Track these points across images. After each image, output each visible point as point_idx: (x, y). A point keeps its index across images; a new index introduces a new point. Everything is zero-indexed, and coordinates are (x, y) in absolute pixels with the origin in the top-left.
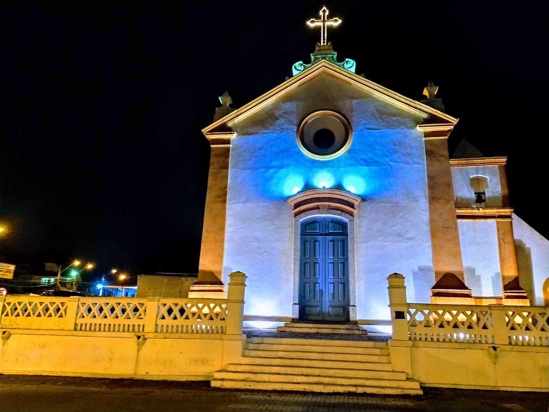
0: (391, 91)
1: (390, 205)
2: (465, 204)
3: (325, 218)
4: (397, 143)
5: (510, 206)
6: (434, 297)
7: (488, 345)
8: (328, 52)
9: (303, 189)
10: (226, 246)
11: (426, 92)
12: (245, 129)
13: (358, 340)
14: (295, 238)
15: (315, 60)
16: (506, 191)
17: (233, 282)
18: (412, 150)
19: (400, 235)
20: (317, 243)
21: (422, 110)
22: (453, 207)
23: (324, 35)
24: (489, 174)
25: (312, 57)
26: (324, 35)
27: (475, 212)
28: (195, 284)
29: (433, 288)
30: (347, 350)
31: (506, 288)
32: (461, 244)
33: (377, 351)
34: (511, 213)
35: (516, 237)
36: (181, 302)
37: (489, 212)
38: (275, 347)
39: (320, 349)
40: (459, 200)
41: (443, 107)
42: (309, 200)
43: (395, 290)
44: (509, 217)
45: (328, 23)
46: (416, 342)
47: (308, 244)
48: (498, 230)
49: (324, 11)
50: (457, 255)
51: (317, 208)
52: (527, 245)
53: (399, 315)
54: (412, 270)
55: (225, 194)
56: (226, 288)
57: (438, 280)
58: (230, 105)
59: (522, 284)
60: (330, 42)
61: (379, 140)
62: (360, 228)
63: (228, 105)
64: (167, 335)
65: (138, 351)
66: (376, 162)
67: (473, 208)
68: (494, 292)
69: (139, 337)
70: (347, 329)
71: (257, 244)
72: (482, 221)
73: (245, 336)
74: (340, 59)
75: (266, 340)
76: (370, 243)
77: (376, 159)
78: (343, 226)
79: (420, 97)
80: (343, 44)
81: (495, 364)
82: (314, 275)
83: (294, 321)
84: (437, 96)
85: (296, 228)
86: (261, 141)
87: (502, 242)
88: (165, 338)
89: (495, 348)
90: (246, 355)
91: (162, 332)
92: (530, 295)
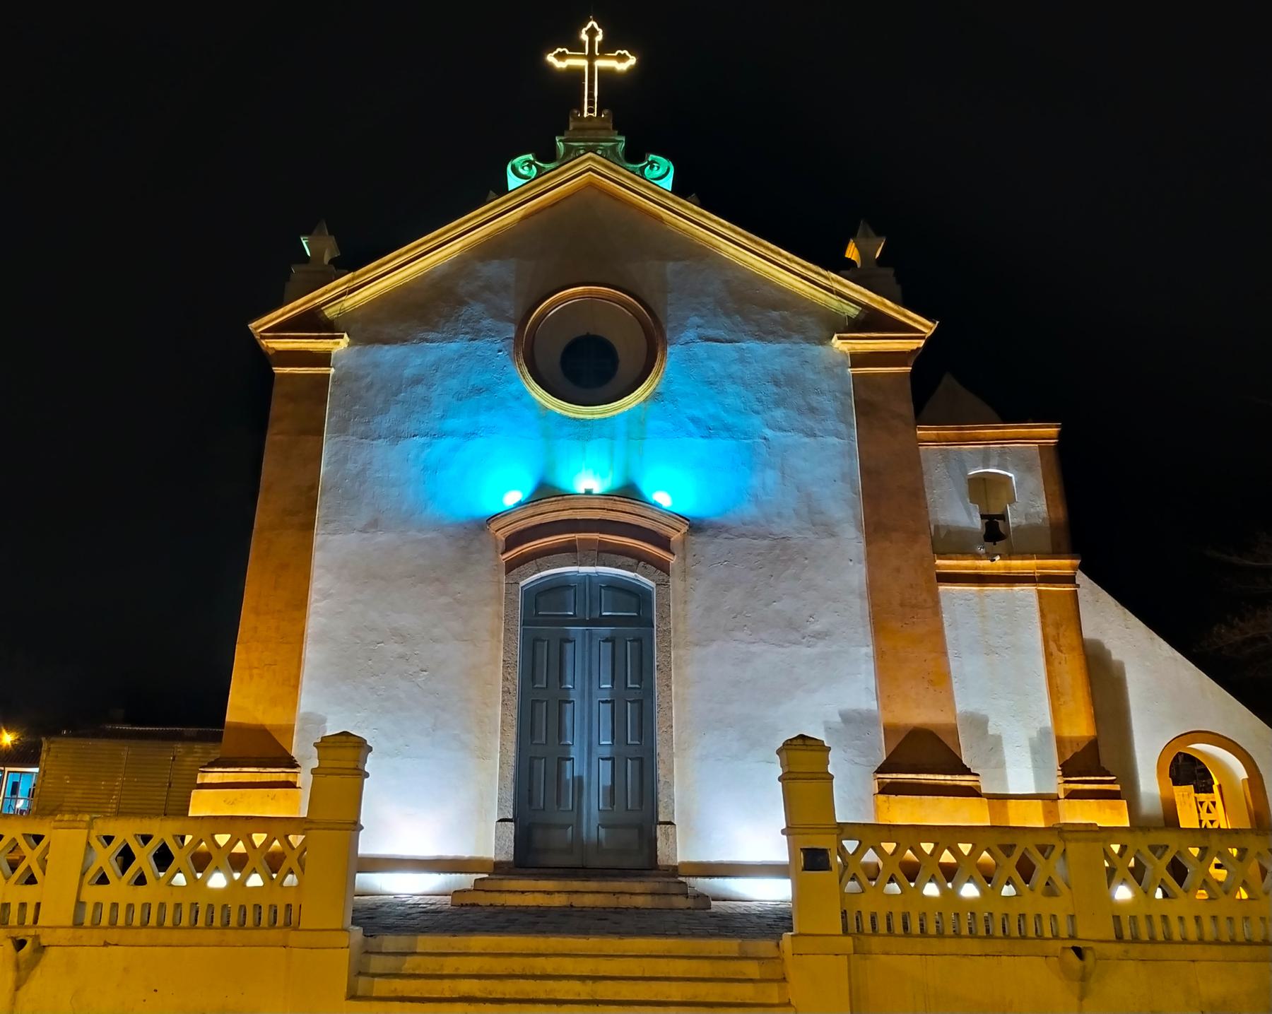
0: (766, 243)
1: (766, 542)
2: (954, 543)
3: (589, 576)
4: (782, 378)
5: (1073, 551)
6: (882, 797)
7: (1058, 945)
8: (602, 134)
9: (533, 494)
10: (311, 653)
11: (852, 253)
12: (374, 326)
13: (693, 935)
14: (507, 630)
15: (566, 154)
16: (1061, 513)
17: (328, 764)
18: (821, 399)
19: (792, 625)
20: (569, 647)
21: (840, 293)
22: (928, 550)
23: (591, 92)
24: (1015, 464)
25: (560, 145)
26: (591, 92)
27: (984, 565)
28: (212, 765)
29: (881, 770)
30: (663, 967)
31: (1069, 769)
32: (950, 652)
33: (752, 969)
34: (1073, 568)
35: (1088, 633)
36: (163, 830)
37: (1019, 565)
38: (450, 965)
39: (586, 967)
40: (943, 533)
41: (897, 289)
42: (552, 525)
43: (799, 785)
44: (1070, 580)
45: (600, 63)
46: (862, 937)
47: (542, 650)
48: (1043, 616)
49: (592, 33)
50: (939, 680)
51: (569, 549)
52: (1116, 656)
53: (814, 860)
54: (826, 723)
55: (313, 507)
56: (304, 778)
57: (892, 748)
58: (331, 262)
59: (1106, 760)
60: (606, 111)
61: (735, 368)
62: (687, 605)
63: (326, 259)
64: (113, 935)
65: (17, 989)
66: (727, 428)
67: (978, 557)
68: (1038, 780)
69: (20, 944)
70: (652, 894)
71: (400, 649)
72: (1002, 589)
73: (358, 931)
74: (635, 155)
75: (425, 942)
76: (714, 646)
77: (730, 420)
78: (640, 597)
79: (840, 265)
80: (640, 119)
81: (1081, 999)
82: (560, 738)
83: (498, 869)
84: (881, 262)
85: (510, 602)
86: (419, 361)
87: (1053, 646)
88: (106, 944)
89: (1079, 952)
90: (359, 993)
91: (96, 924)
92: (1127, 792)
